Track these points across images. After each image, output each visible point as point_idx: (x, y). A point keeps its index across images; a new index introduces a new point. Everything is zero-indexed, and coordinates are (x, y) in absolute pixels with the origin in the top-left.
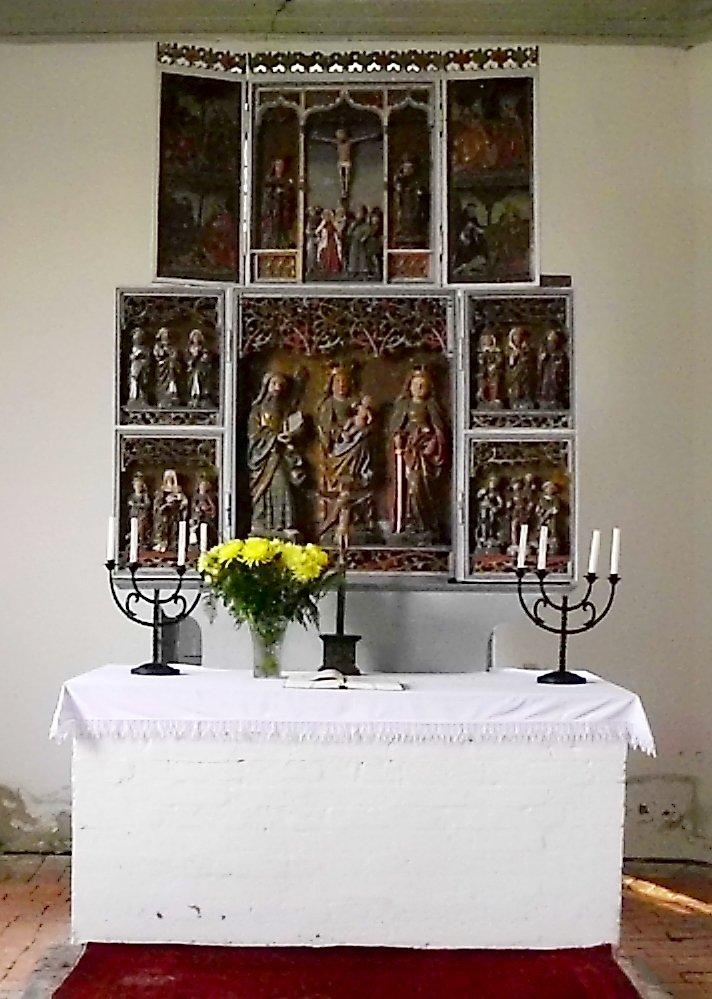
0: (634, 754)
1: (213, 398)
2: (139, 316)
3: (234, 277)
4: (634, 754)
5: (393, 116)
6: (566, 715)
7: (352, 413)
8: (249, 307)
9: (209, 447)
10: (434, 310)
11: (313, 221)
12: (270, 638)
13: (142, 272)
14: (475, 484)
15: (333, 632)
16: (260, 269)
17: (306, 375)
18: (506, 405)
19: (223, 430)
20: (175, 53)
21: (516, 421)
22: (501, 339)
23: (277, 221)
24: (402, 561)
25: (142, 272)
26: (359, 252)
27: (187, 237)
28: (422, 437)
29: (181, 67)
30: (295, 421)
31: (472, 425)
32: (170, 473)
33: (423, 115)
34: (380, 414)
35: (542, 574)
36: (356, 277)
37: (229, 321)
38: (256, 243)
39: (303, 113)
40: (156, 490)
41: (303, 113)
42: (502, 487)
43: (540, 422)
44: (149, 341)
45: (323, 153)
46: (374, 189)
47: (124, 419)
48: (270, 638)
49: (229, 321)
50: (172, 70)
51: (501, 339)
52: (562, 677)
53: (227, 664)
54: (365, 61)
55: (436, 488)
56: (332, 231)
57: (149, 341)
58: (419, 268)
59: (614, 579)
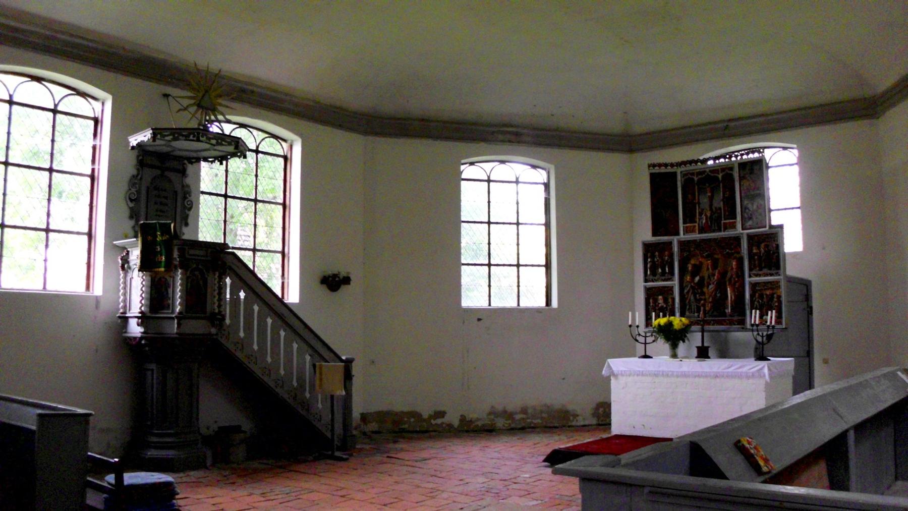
0: (766, 382)
1: (672, 273)
2: (648, 249)
3: (678, 234)
4: (766, 382)
5: (723, 176)
6: (745, 369)
7: (714, 275)
8: (682, 244)
9: (671, 289)
10: (737, 239)
11: (701, 214)
12: (674, 346)
13: (648, 237)
14: (752, 296)
15: (700, 345)
16: (687, 231)
17: (701, 263)
18: (761, 270)
19: (675, 283)
20: (654, 166)
21: (766, 275)
22: (759, 248)
23: (689, 217)
24: (731, 323)
25: (648, 237)
26: (714, 223)
27: (662, 221)
28: (736, 282)
29: (657, 170)
30: (697, 279)
31: (750, 276)
32: (660, 297)
33: (732, 175)
34: (723, 274)
35: (757, 325)
36: (714, 231)
37: (676, 249)
38: (684, 223)
39: (696, 179)
40: (656, 301)
41: (720, 176)
42: (761, 296)
43: (771, 275)
44: (653, 257)
45: (702, 191)
46: (718, 203)
47: (646, 281)
48: (674, 346)
49: (676, 249)
50: (654, 171)
51: (759, 248)
52: (646, 356)
53: (658, 354)
54: (724, 157)
55: (740, 297)
56: (706, 215)
57: (653, 257)
58: (733, 226)
59: (638, 327)
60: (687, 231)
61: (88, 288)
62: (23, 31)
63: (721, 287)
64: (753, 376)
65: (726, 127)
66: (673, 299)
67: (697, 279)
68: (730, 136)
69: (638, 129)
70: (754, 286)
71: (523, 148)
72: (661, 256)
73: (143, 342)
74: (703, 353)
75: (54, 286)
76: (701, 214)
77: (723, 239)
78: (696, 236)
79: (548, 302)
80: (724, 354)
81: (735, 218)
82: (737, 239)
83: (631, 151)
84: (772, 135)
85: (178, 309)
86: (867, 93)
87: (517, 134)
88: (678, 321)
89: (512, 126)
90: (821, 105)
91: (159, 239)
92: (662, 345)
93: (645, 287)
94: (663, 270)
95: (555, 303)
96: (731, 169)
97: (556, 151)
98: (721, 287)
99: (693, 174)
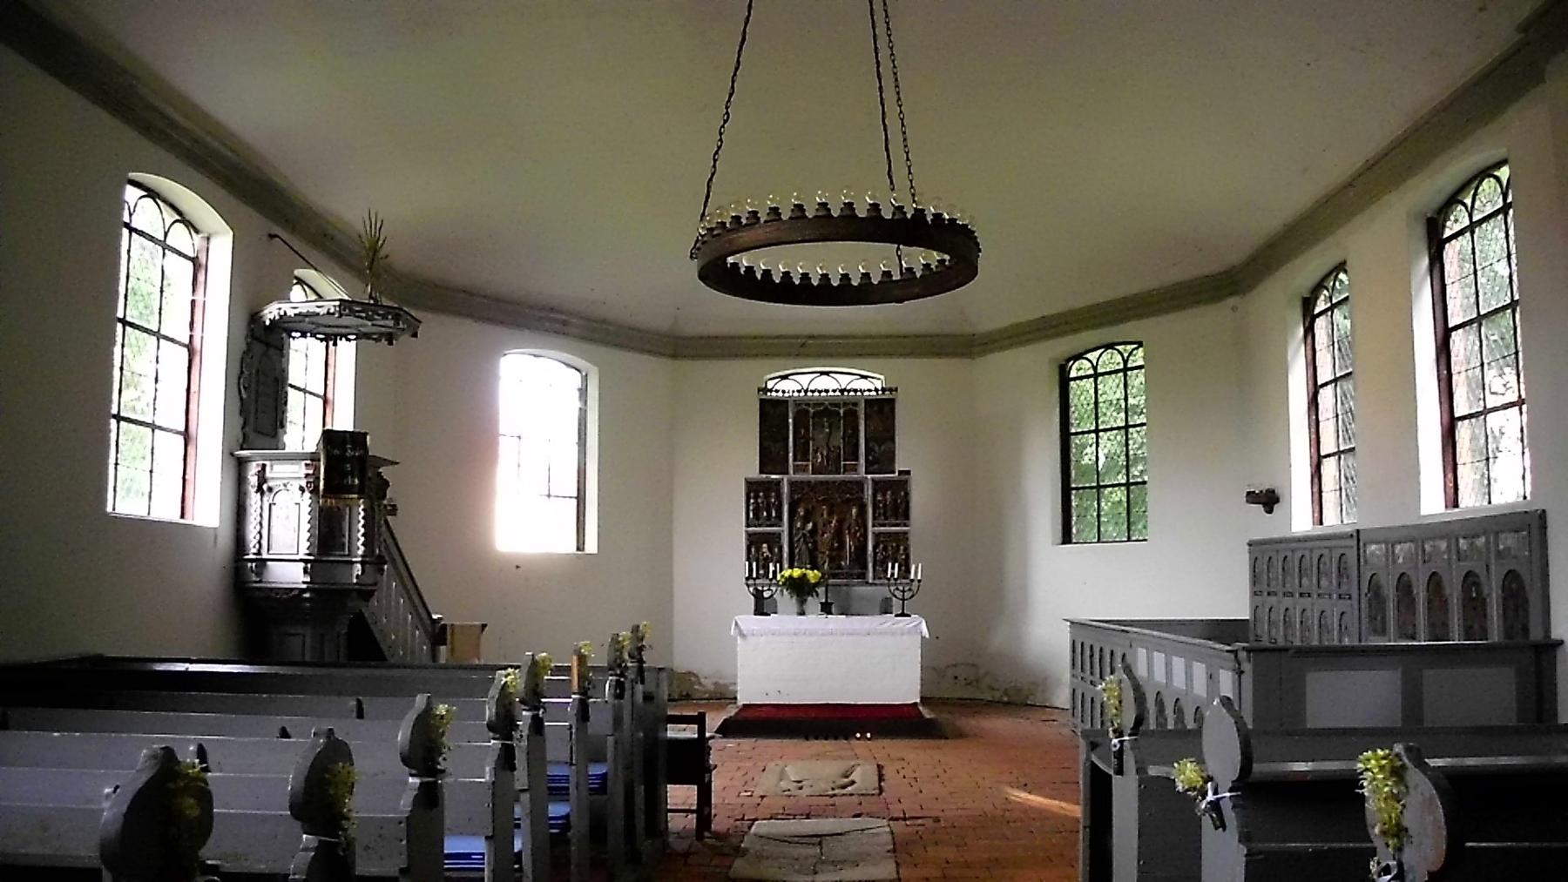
2: (752, 487)
8: (792, 484)
9: (779, 535)
10: (860, 484)
11: (816, 452)
12: (802, 602)
13: (754, 473)
14: (875, 548)
16: (797, 469)
22: (884, 495)
23: (802, 453)
24: (850, 576)
26: (832, 464)
27: (771, 458)
30: (810, 526)
37: (785, 489)
42: (885, 549)
46: (838, 441)
47: (748, 526)
48: (802, 602)
49: (785, 489)
51: (884, 495)
57: (756, 497)
58: (854, 469)
60: (797, 469)
61: (182, 516)
62: (164, 117)
63: (838, 535)
64: (909, 632)
65: (803, 345)
66: (781, 549)
67: (810, 526)
68: (808, 356)
69: (690, 329)
70: (877, 535)
71: (561, 340)
72: (767, 497)
73: (307, 595)
74: (826, 609)
75: (156, 515)
76: (816, 452)
77: (843, 482)
78: (809, 476)
79: (580, 546)
80: (845, 612)
81: (857, 459)
82: (860, 484)
83: (674, 356)
84: (857, 361)
85: (360, 552)
86: (968, 329)
87: (565, 323)
88: (813, 575)
89: (561, 312)
90: (917, 336)
91: (349, 453)
92: (785, 599)
93: (749, 535)
94: (769, 514)
95: (591, 546)
96: (855, 404)
97: (603, 351)
98: (838, 535)
99: (837, 405)
